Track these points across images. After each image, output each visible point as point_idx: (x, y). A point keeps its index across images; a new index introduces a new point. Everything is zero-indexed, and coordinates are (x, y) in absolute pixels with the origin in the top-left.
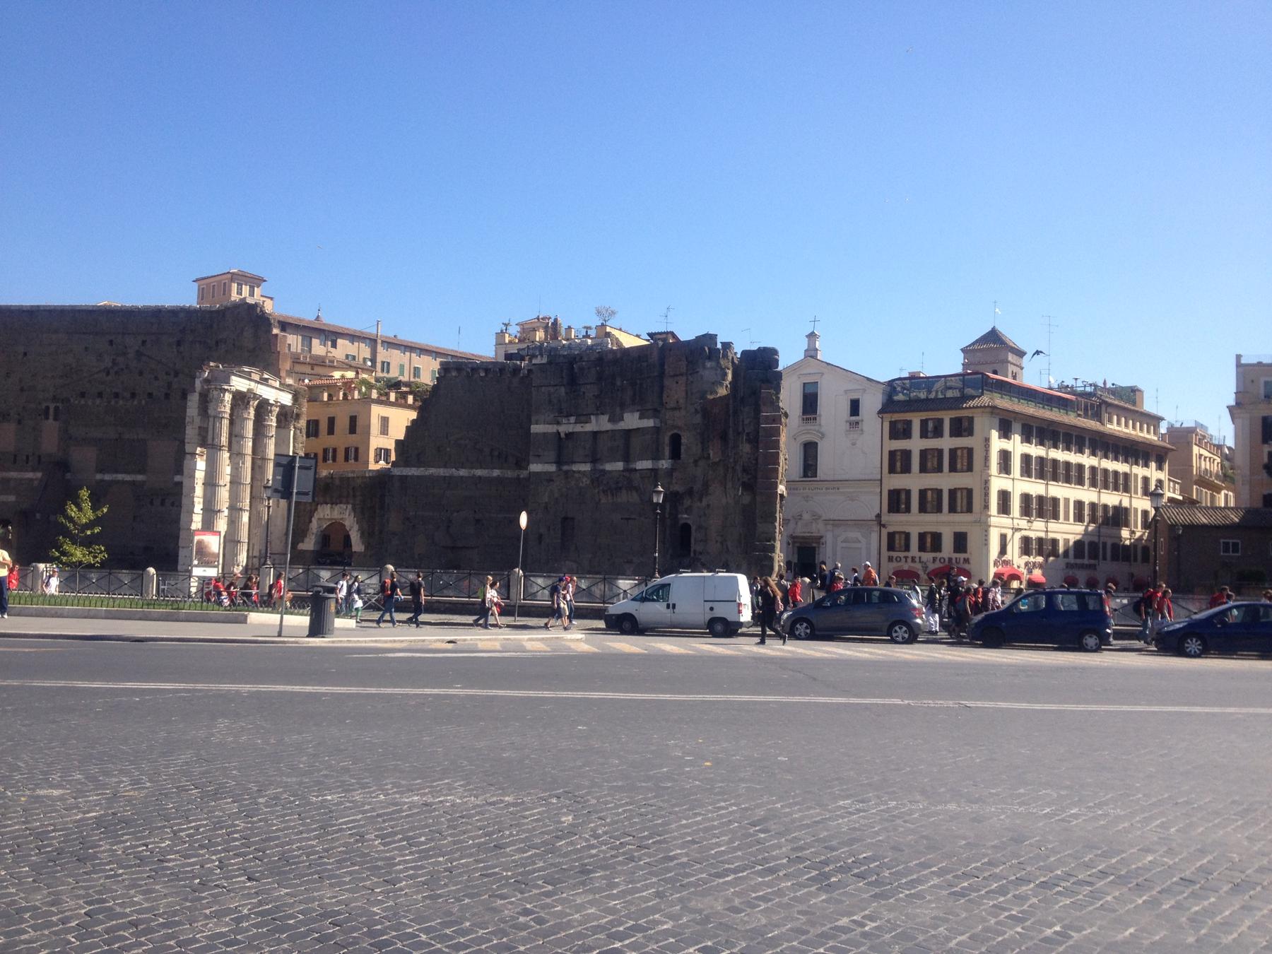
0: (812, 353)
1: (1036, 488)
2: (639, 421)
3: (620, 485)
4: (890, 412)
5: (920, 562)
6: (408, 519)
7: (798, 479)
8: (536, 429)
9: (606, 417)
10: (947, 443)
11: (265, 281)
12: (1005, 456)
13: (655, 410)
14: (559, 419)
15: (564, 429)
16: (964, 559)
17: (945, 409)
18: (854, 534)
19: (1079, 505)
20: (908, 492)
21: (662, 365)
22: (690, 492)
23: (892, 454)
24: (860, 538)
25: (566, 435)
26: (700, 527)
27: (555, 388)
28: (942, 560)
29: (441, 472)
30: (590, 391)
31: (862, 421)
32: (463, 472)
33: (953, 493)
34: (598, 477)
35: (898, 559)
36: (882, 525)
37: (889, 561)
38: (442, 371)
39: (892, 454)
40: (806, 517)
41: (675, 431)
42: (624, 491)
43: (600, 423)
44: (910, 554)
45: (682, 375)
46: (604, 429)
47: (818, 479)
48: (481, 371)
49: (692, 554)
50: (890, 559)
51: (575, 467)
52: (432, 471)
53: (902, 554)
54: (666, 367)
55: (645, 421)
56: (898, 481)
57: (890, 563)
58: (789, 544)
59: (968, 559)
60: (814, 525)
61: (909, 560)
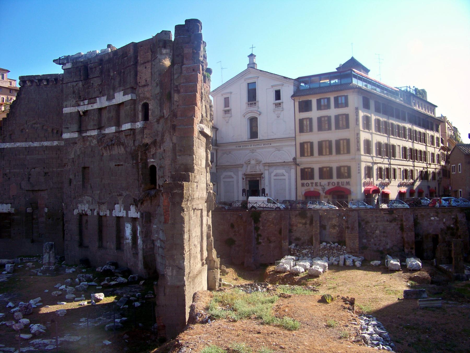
0: (252, 66)
1: (383, 139)
2: (123, 97)
3: (113, 142)
4: (298, 96)
5: (320, 185)
6: (6, 174)
7: (247, 140)
8: (66, 110)
9: (105, 98)
10: (333, 112)
11: (9, 71)
12: (367, 120)
13: (132, 88)
14: (79, 102)
15: (82, 109)
16: (347, 182)
17: (331, 92)
18: (281, 171)
19: (405, 149)
20: (312, 144)
21: (136, 57)
22: (155, 143)
23: (301, 121)
24: (285, 173)
25: (83, 112)
26: (161, 167)
27: (76, 83)
28: (333, 184)
29: (23, 144)
30: (96, 82)
31: (282, 103)
32: (36, 144)
33: (338, 142)
34: (101, 138)
35: (308, 185)
36: (297, 165)
37: (302, 186)
38: (21, 83)
39: (301, 121)
40: (253, 162)
41: (145, 101)
42: (116, 147)
43: (102, 102)
44: (314, 181)
45: (148, 62)
46: (104, 106)
47: (258, 139)
48: (44, 81)
49: (158, 188)
50: (303, 185)
51: (89, 133)
52: (18, 144)
53: (309, 181)
54: (139, 58)
55: (126, 96)
56: (305, 137)
57: (303, 188)
58: (243, 179)
59: (349, 182)
60: (257, 167)
61: (314, 185)
